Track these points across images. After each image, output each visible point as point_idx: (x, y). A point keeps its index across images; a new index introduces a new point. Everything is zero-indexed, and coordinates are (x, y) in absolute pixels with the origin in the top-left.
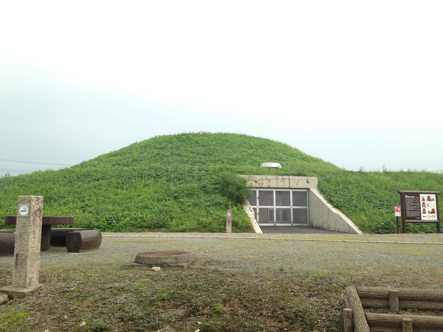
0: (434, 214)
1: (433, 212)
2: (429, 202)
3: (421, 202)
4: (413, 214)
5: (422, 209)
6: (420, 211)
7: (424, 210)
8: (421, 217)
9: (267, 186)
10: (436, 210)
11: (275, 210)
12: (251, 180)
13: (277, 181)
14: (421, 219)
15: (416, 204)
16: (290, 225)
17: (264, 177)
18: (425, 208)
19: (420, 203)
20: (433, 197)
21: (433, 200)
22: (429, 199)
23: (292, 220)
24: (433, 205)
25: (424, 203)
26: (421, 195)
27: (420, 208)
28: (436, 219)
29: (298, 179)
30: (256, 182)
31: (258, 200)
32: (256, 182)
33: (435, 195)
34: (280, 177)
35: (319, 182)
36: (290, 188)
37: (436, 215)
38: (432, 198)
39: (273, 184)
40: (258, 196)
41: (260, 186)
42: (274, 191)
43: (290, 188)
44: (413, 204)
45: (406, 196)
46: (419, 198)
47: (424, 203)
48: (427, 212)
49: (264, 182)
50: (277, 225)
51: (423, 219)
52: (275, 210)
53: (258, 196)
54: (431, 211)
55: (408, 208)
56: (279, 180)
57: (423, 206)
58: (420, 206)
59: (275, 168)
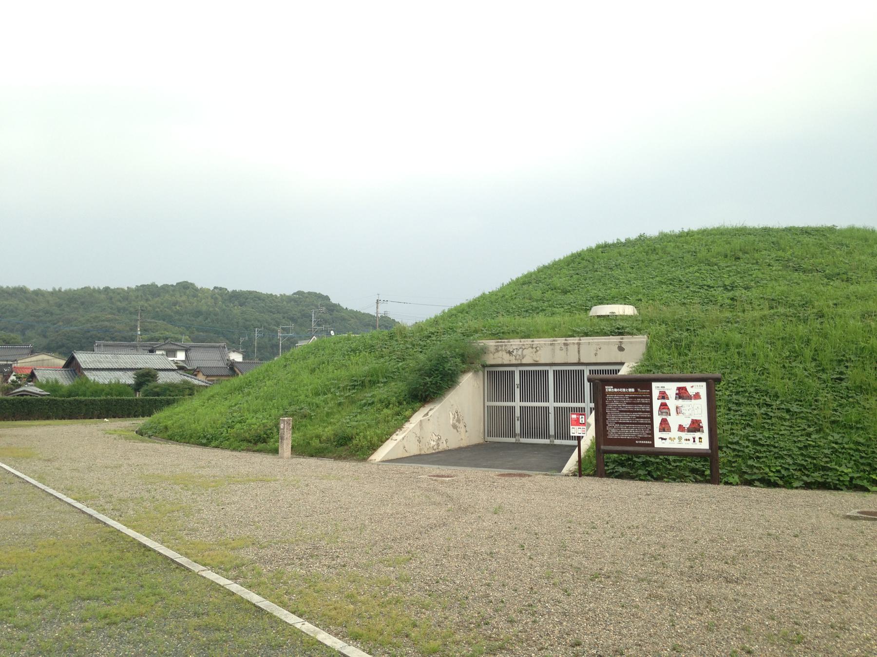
0: (697, 435)
1: (695, 426)
2: (680, 402)
4: (627, 433)
5: (657, 420)
6: (652, 424)
8: (652, 439)
9: (532, 362)
10: (705, 424)
11: (552, 411)
13: (553, 350)
14: (653, 445)
15: (637, 408)
16: (547, 441)
17: (528, 341)
18: (669, 418)
20: (701, 388)
21: (697, 396)
22: (682, 394)
23: (552, 432)
24: (699, 410)
26: (654, 385)
27: (652, 418)
28: (705, 445)
29: (598, 344)
30: (510, 353)
31: (517, 392)
32: (510, 353)
33: (704, 384)
34: (561, 340)
35: (649, 348)
36: (579, 364)
37: (705, 435)
39: (544, 356)
42: (551, 370)
43: (579, 364)
44: (630, 407)
45: (609, 389)
46: (651, 393)
48: (674, 426)
49: (525, 352)
50: (557, 442)
51: (658, 444)
52: (552, 411)
54: (687, 424)
55: (612, 418)
56: (557, 347)
57: (661, 412)
58: (651, 412)
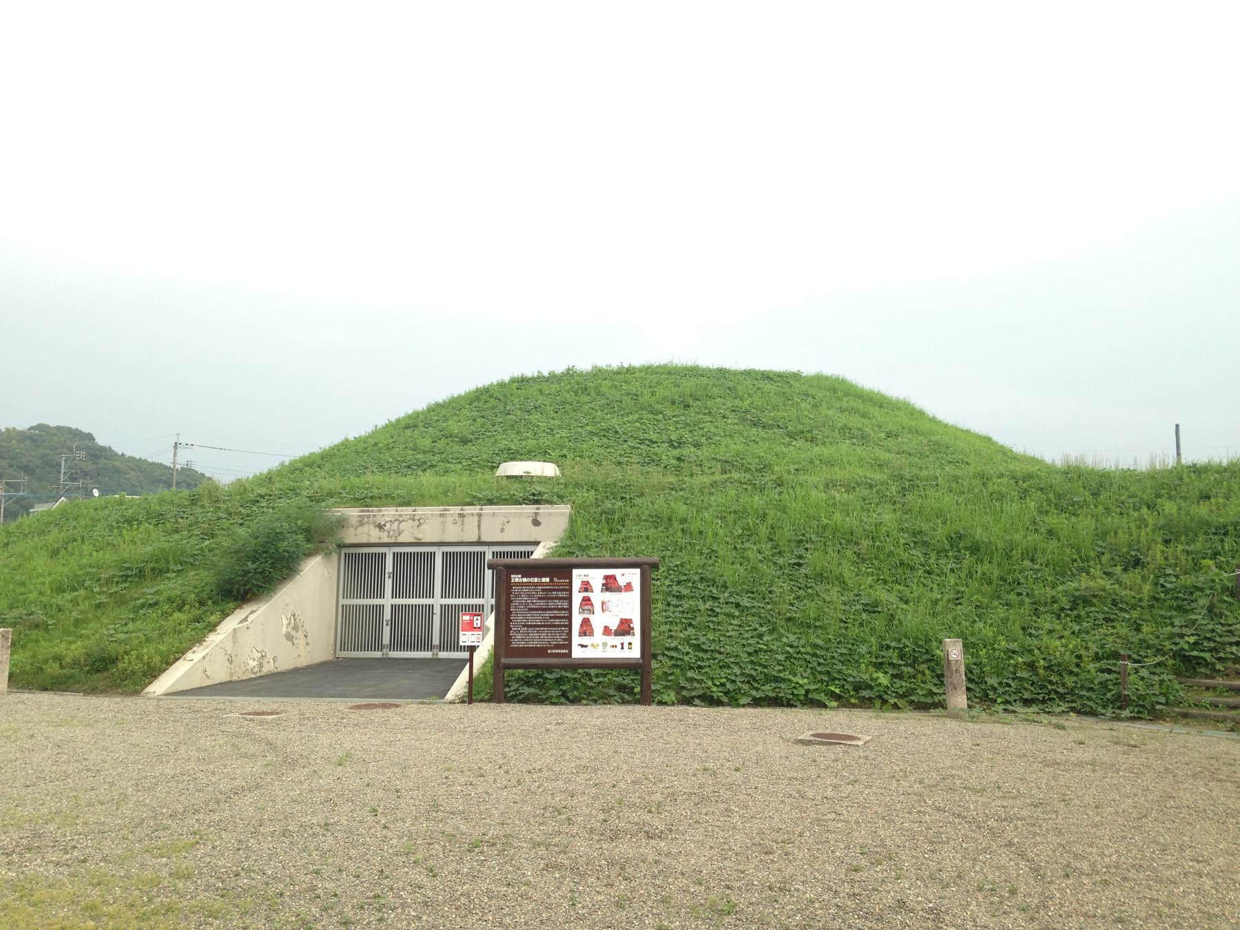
1: (624, 628)
2: (608, 596)
3: (577, 598)
4: (537, 639)
6: (570, 626)
7: (586, 622)
8: (569, 647)
11: (437, 610)
12: (368, 523)
13: (444, 523)
15: (551, 604)
16: (427, 654)
17: (408, 511)
18: (592, 618)
19: (570, 599)
20: (632, 576)
21: (629, 587)
22: (610, 585)
24: (628, 605)
25: (586, 600)
26: (575, 572)
28: (635, 653)
30: (380, 527)
31: (389, 583)
32: (380, 527)
33: (638, 571)
34: (455, 510)
37: (636, 640)
38: (622, 581)
39: (430, 532)
40: (389, 568)
41: (393, 540)
44: (542, 603)
45: (516, 578)
47: (586, 600)
48: (598, 628)
49: (403, 526)
50: (443, 655)
51: (577, 653)
52: (437, 610)
53: (389, 568)
55: (518, 618)
56: (449, 520)
57: (582, 610)
58: (570, 609)
59: (516, 477)
